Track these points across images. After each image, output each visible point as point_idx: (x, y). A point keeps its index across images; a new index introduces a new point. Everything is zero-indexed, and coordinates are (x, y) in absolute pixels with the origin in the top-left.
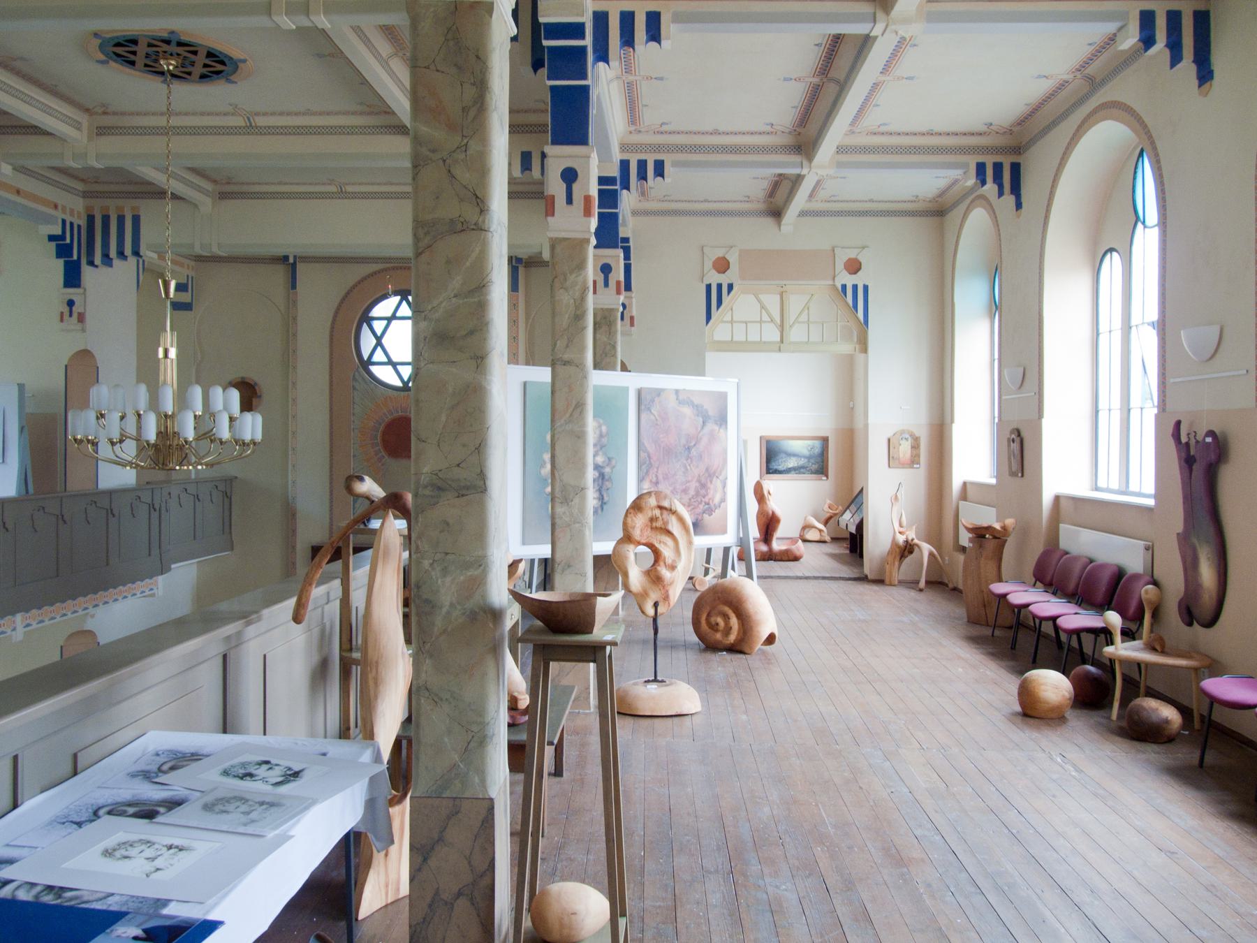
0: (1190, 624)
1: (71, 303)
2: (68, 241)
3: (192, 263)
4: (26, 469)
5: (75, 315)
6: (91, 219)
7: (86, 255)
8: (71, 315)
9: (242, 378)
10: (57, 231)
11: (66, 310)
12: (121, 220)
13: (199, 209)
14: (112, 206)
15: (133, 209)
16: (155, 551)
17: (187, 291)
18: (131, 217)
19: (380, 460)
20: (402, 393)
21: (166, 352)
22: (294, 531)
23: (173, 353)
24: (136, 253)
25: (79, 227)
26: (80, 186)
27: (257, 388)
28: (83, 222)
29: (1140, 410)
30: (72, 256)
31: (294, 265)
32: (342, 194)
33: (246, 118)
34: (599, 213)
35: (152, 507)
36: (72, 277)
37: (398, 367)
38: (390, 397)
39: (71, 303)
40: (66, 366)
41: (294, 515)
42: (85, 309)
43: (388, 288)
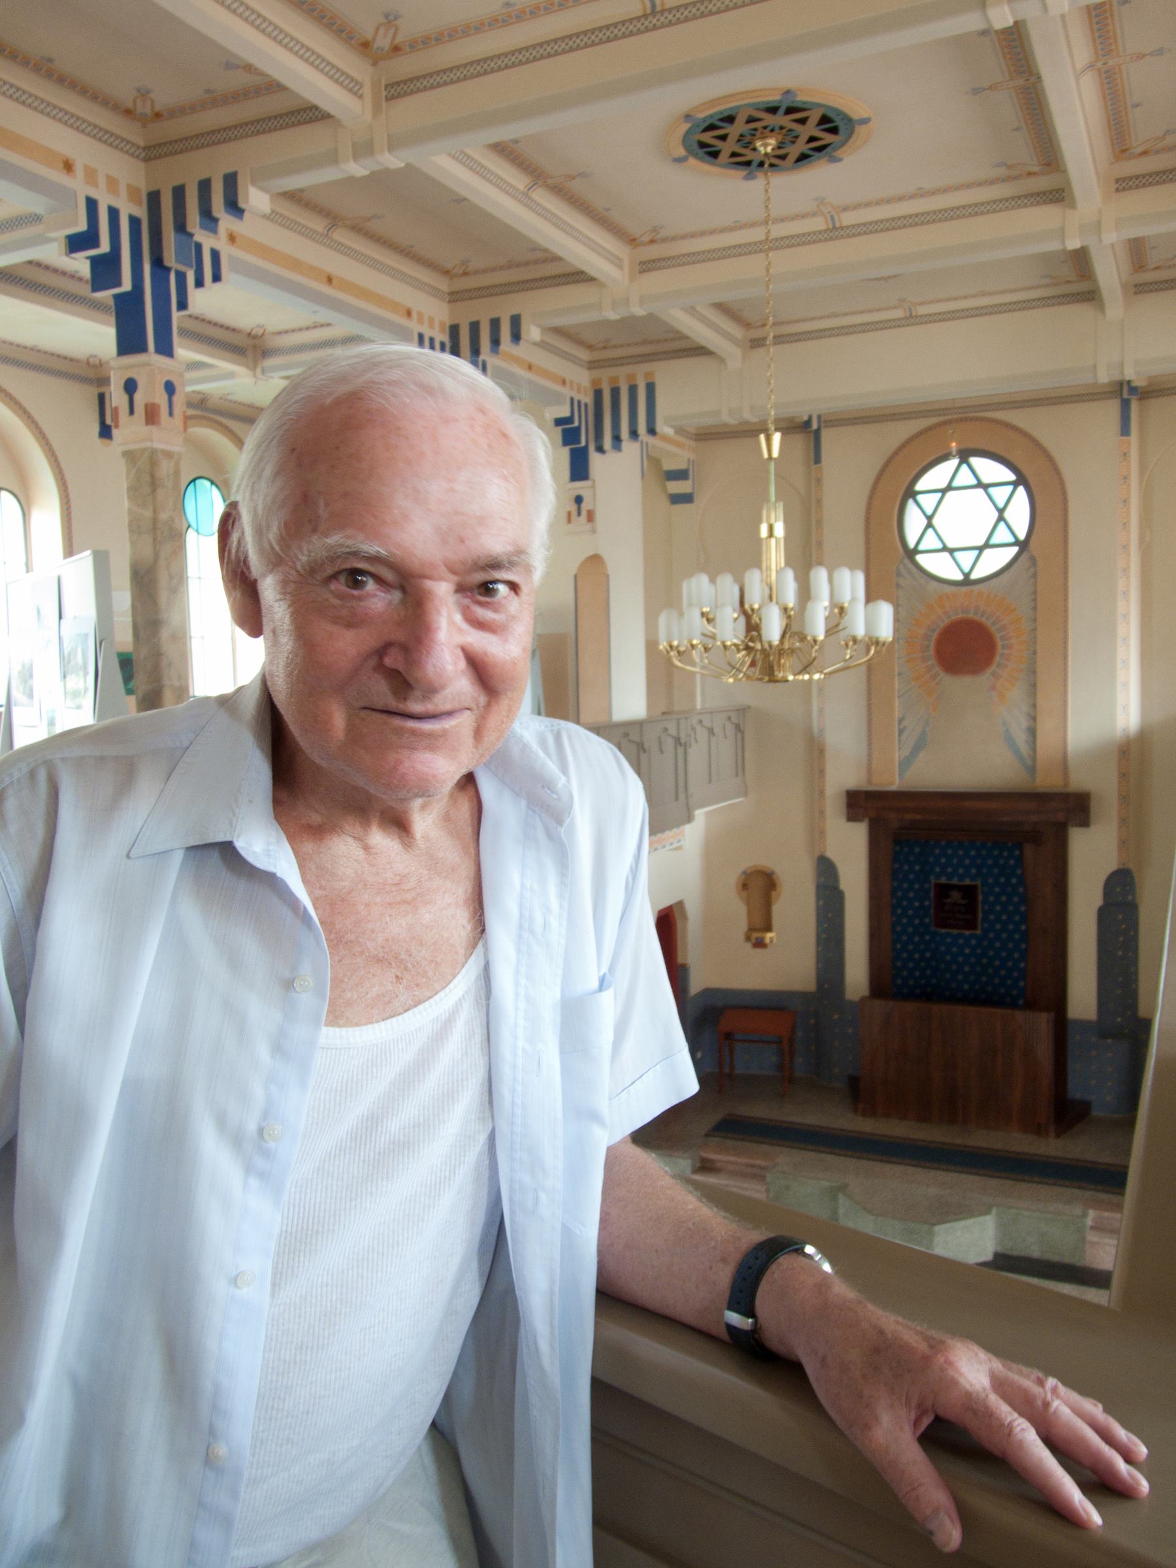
1: (579, 500)
2: (576, 424)
3: (692, 443)
5: (584, 513)
6: (598, 394)
7: (594, 439)
8: (579, 514)
10: (565, 412)
11: (573, 508)
12: (633, 390)
14: (622, 374)
16: (682, 796)
19: (934, 677)
20: (964, 589)
21: (771, 529)
22: (822, 772)
23: (779, 530)
24: (652, 431)
25: (586, 405)
26: (584, 355)
28: (588, 399)
29: (131, 855)
30: (579, 442)
31: (817, 433)
32: (912, 320)
33: (829, 218)
35: (677, 741)
36: (579, 469)
39: (579, 500)
40: (576, 577)
41: (822, 751)
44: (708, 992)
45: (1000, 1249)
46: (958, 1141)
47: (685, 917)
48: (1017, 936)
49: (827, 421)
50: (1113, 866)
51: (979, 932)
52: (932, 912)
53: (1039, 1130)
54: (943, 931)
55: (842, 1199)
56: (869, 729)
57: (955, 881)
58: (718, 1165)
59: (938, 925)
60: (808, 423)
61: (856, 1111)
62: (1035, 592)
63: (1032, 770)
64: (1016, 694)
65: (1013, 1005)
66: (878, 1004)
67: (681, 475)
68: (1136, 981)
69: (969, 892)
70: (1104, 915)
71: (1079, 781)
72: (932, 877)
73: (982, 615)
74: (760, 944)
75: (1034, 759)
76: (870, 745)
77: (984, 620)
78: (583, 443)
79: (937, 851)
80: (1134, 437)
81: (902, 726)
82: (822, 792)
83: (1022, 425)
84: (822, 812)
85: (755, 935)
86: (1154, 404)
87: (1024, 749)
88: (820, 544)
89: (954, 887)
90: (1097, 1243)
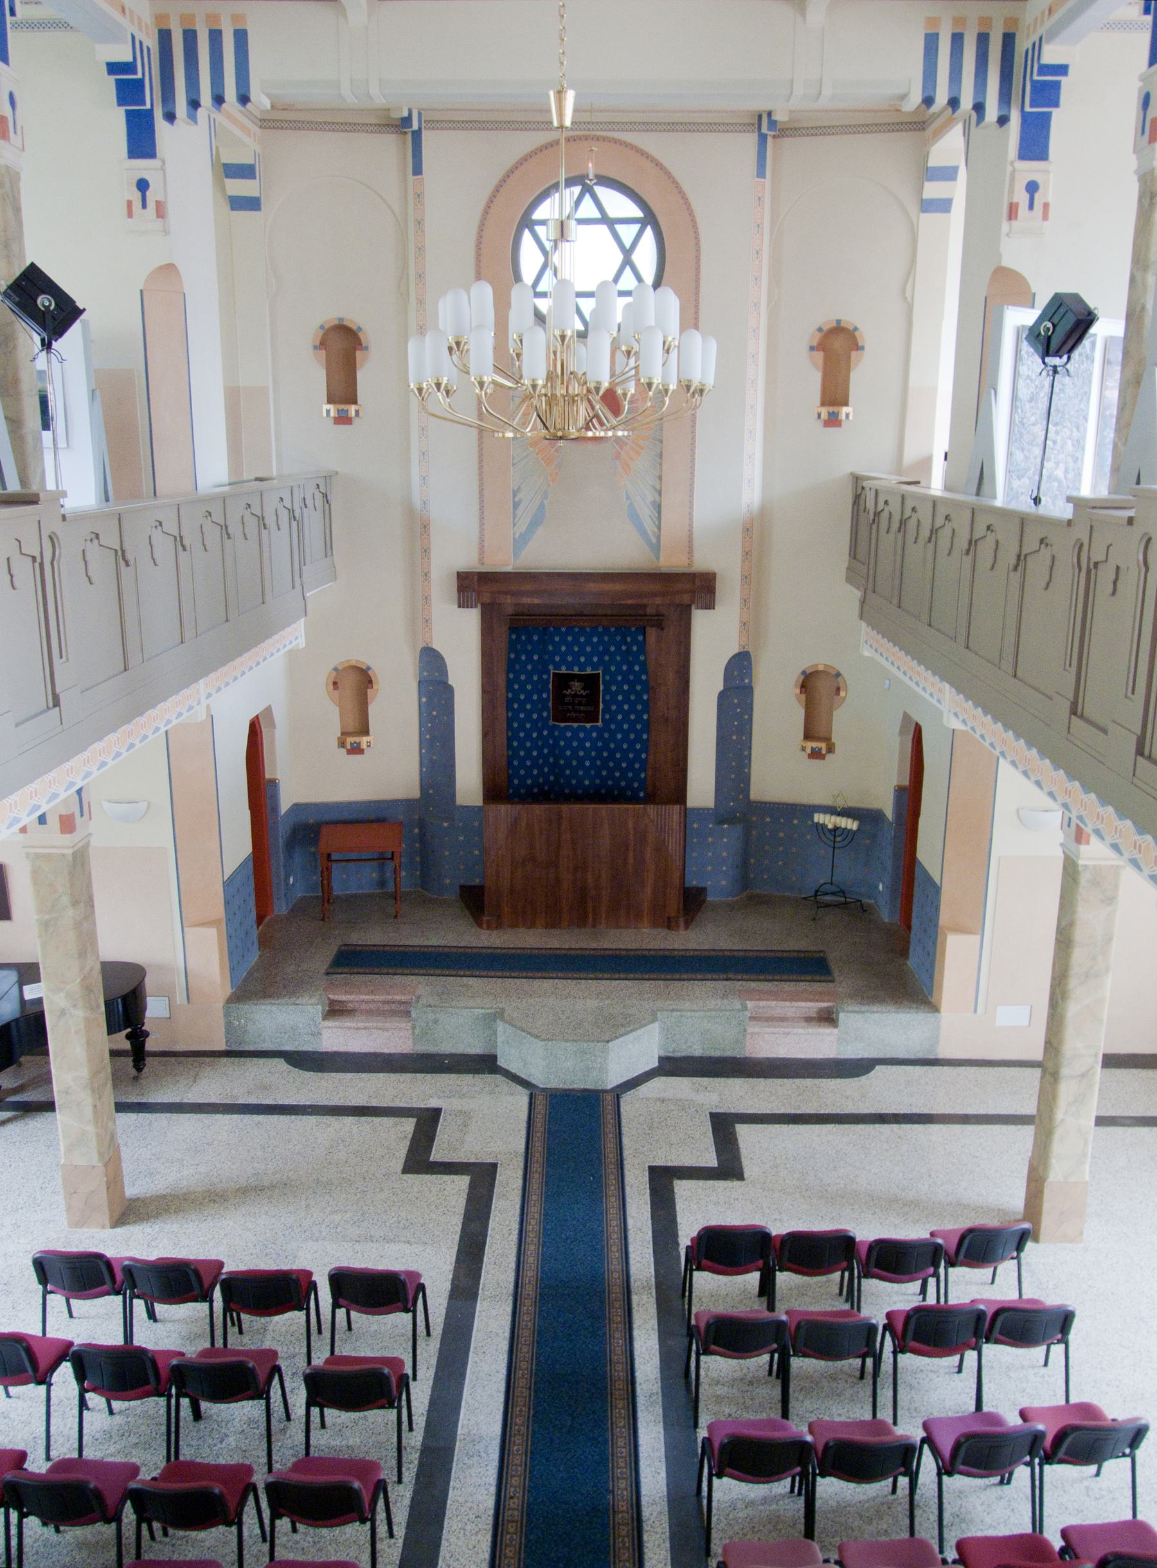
0: (861, 619)
1: (143, 185)
3: (258, 131)
4: (982, 468)
6: (165, 37)
8: (144, 206)
10: (123, 54)
11: (136, 196)
13: (346, 18)
15: (236, 18)
17: (255, 178)
18: (232, 32)
22: (426, 551)
27: (361, 335)
28: (151, 42)
41: (425, 527)
42: (166, 195)
43: (588, 167)
44: (297, 808)
45: (663, 1054)
46: (594, 945)
47: (272, 725)
48: (639, 727)
49: (429, 121)
51: (600, 724)
52: (550, 705)
53: (670, 924)
55: (500, 1026)
57: (576, 670)
58: (350, 1006)
60: (406, 121)
61: (480, 925)
63: (656, 548)
65: (634, 799)
66: (504, 810)
67: (245, 172)
69: (591, 682)
71: (702, 562)
74: (356, 750)
75: (658, 538)
76: (482, 519)
80: (768, 181)
81: (517, 499)
82: (426, 575)
84: (427, 598)
85: (350, 740)
86: (786, 142)
87: (649, 526)
88: (420, 276)
90: (758, 1033)
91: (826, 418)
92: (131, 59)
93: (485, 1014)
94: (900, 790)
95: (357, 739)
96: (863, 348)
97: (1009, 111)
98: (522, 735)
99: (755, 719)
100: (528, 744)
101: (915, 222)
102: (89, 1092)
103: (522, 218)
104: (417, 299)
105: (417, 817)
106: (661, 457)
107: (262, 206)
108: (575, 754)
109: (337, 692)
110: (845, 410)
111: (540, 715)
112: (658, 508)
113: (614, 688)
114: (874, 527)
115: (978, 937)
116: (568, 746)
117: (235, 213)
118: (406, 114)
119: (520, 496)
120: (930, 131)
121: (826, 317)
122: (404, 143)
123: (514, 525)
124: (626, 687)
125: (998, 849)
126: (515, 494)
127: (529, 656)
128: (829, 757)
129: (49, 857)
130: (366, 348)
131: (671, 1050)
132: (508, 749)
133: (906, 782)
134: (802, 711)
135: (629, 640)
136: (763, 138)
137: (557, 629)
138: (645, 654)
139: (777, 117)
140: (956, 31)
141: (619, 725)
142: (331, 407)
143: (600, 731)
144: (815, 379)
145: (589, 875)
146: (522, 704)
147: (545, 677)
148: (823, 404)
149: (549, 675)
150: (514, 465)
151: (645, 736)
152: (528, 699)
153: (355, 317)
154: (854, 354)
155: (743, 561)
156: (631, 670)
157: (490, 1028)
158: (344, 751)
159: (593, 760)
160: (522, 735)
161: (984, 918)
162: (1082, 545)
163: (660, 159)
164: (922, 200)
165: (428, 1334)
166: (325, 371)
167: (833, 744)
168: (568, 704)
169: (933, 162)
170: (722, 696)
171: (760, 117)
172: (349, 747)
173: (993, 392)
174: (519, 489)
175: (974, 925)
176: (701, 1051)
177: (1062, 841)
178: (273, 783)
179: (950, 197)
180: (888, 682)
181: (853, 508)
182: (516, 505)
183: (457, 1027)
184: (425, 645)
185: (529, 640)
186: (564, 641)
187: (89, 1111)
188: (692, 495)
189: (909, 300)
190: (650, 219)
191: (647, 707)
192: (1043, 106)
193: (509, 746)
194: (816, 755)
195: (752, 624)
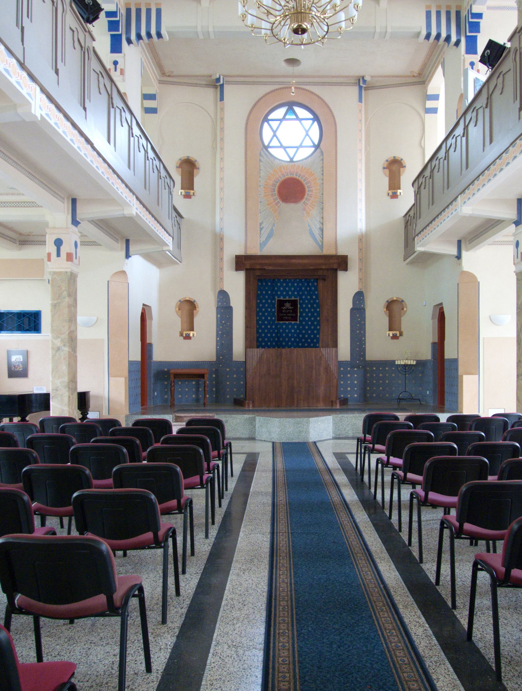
7: (125, 34)
9: (188, 157)
19: (277, 204)
22: (222, 249)
27: (196, 163)
31: (222, 86)
34: (130, 462)
37: (287, 149)
38: (283, 166)
41: (222, 239)
42: (125, 66)
49: (227, 81)
50: (357, 290)
51: (298, 322)
52: (276, 314)
54: (281, 322)
56: (246, 227)
57: (287, 298)
59: (278, 320)
60: (218, 80)
62: (323, 167)
63: (322, 247)
64: (315, 212)
68: (365, 344)
69: (294, 303)
70: (353, 311)
71: (341, 252)
72: (276, 297)
73: (299, 176)
74: (188, 337)
75: (322, 242)
77: (300, 178)
78: (120, 33)
79: (279, 284)
80: (363, 104)
81: (261, 227)
82: (222, 259)
83: (317, 92)
86: (371, 92)
87: (318, 238)
89: (286, 301)
91: (392, 194)
92: (115, 10)
93: (250, 418)
94: (434, 344)
95: (188, 332)
96: (405, 167)
97: (461, 37)
98: (263, 318)
99: (367, 323)
100: (266, 331)
101: (423, 117)
102: (67, 389)
103: (265, 117)
104: (220, 148)
105: (214, 369)
106: (323, 209)
107: (158, 112)
108: (287, 336)
109: (180, 311)
110: (399, 191)
111: (271, 318)
112: (322, 230)
113: (304, 306)
114: (418, 195)
115: (477, 376)
116: (284, 331)
117: (147, 114)
118: (218, 77)
119: (263, 225)
120: (426, 84)
121: (390, 156)
122: (217, 93)
123: (260, 237)
124: (309, 306)
125: (483, 334)
126: (261, 224)
127: (267, 291)
128: (401, 338)
129: (60, 273)
130: (198, 168)
131: (338, 434)
132: (257, 342)
133: (436, 341)
134: (388, 318)
135: (310, 284)
136: (360, 88)
137: (279, 280)
138: (317, 291)
139: (367, 78)
140: (438, 10)
141: (307, 322)
142: (183, 191)
143: (298, 326)
144: (386, 180)
145: (295, 382)
146: (263, 313)
147: (273, 302)
148: (389, 189)
149: (275, 301)
150: (260, 213)
151: (318, 319)
152: (266, 311)
153: (193, 156)
154: (401, 169)
155: (359, 253)
156: (311, 298)
157: (252, 424)
158: (182, 338)
159: (295, 338)
160: (263, 335)
161: (479, 367)
162: (517, 50)
163: (320, 95)
164: (426, 108)
165: (232, 475)
166: (180, 177)
167: (402, 332)
168: (284, 313)
169: (429, 93)
170: (352, 310)
171: (359, 80)
172: (184, 335)
173: (466, 100)
174: (262, 222)
175: (475, 370)
176: (352, 434)
177: (515, 270)
178: (150, 345)
179: (437, 107)
180: (424, 302)
181: (405, 230)
182: (261, 229)
183: (236, 425)
184: (220, 289)
185: (267, 285)
186: (282, 286)
187: (66, 399)
188: (336, 225)
189: (423, 147)
190: (316, 118)
191: (319, 315)
192: (474, 32)
193: (258, 332)
194: (395, 337)
195: (364, 278)
